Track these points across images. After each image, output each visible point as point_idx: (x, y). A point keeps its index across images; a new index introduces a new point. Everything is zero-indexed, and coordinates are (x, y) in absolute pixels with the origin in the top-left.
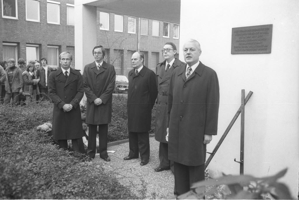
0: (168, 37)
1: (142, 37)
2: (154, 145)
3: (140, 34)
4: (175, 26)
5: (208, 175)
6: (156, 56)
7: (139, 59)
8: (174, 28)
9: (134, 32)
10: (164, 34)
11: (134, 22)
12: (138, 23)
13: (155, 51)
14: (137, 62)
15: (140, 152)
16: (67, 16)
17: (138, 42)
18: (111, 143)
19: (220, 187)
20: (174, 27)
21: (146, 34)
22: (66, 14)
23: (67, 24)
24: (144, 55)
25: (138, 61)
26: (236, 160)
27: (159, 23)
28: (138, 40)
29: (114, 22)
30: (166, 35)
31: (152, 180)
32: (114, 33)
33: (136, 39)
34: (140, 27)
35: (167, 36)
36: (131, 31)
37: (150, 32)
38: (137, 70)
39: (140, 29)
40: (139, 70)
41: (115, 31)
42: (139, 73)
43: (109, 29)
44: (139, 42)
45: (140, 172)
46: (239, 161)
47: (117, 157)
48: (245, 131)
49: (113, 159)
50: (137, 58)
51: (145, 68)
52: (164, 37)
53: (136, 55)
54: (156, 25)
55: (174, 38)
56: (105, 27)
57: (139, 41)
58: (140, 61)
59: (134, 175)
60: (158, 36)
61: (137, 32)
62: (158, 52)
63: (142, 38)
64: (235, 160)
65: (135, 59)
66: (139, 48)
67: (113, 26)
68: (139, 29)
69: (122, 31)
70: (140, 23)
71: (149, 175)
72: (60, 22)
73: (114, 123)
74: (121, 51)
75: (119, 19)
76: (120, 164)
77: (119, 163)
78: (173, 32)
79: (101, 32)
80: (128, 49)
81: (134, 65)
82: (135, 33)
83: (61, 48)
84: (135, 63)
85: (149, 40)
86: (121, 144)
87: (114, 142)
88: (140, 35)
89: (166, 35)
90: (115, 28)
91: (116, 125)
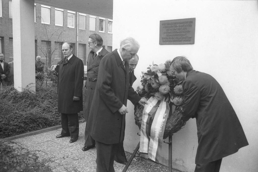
0: (104, 32)
1: (80, 32)
2: (82, 127)
3: (78, 28)
4: (110, 23)
5: (140, 155)
6: (83, 48)
7: (69, 49)
8: (109, 24)
9: (62, 25)
10: (100, 29)
11: (73, 18)
12: (77, 19)
13: (82, 43)
14: (69, 52)
15: (70, 133)
16: (10, 9)
17: (77, 36)
18: (50, 128)
19: (151, 166)
20: (108, 23)
21: (84, 29)
22: (8, 8)
23: (10, 17)
24: (72, 46)
25: (68, 51)
26: (165, 142)
27: (95, 19)
28: (77, 34)
29: (54, 17)
30: (102, 30)
31: (88, 163)
32: (54, 27)
33: (75, 33)
34: (79, 22)
35: (103, 31)
36: (71, 26)
37: (87, 25)
38: (67, 59)
39: (79, 25)
40: (69, 59)
41: (56, 25)
42: (68, 62)
43: (62, 25)
44: (78, 36)
45: (77, 156)
46: (168, 142)
47: (55, 142)
48: (156, 112)
49: (50, 144)
50: (67, 49)
51: (74, 57)
52: (100, 31)
53: (65, 46)
54: (93, 20)
55: (109, 33)
56: (46, 20)
57: (78, 35)
58: (70, 51)
59: (70, 159)
60: (95, 30)
61: (76, 26)
62: (85, 44)
63: (80, 33)
64: (138, 134)
65: (66, 50)
66: (78, 41)
67: (54, 21)
68: (78, 24)
69: (62, 25)
70: (79, 19)
71: (86, 158)
72: (2, 15)
73: (53, 109)
74: (49, 43)
75: (59, 13)
76: (57, 149)
77: (46, 144)
78: (108, 28)
79: (43, 26)
80: (54, 41)
81: (65, 55)
82: (74, 27)
83: (4, 39)
84: (66, 53)
85: (86, 34)
86: (59, 129)
87: (52, 127)
88: (79, 29)
89: (102, 30)
90: (55, 23)
91: (54, 111)
